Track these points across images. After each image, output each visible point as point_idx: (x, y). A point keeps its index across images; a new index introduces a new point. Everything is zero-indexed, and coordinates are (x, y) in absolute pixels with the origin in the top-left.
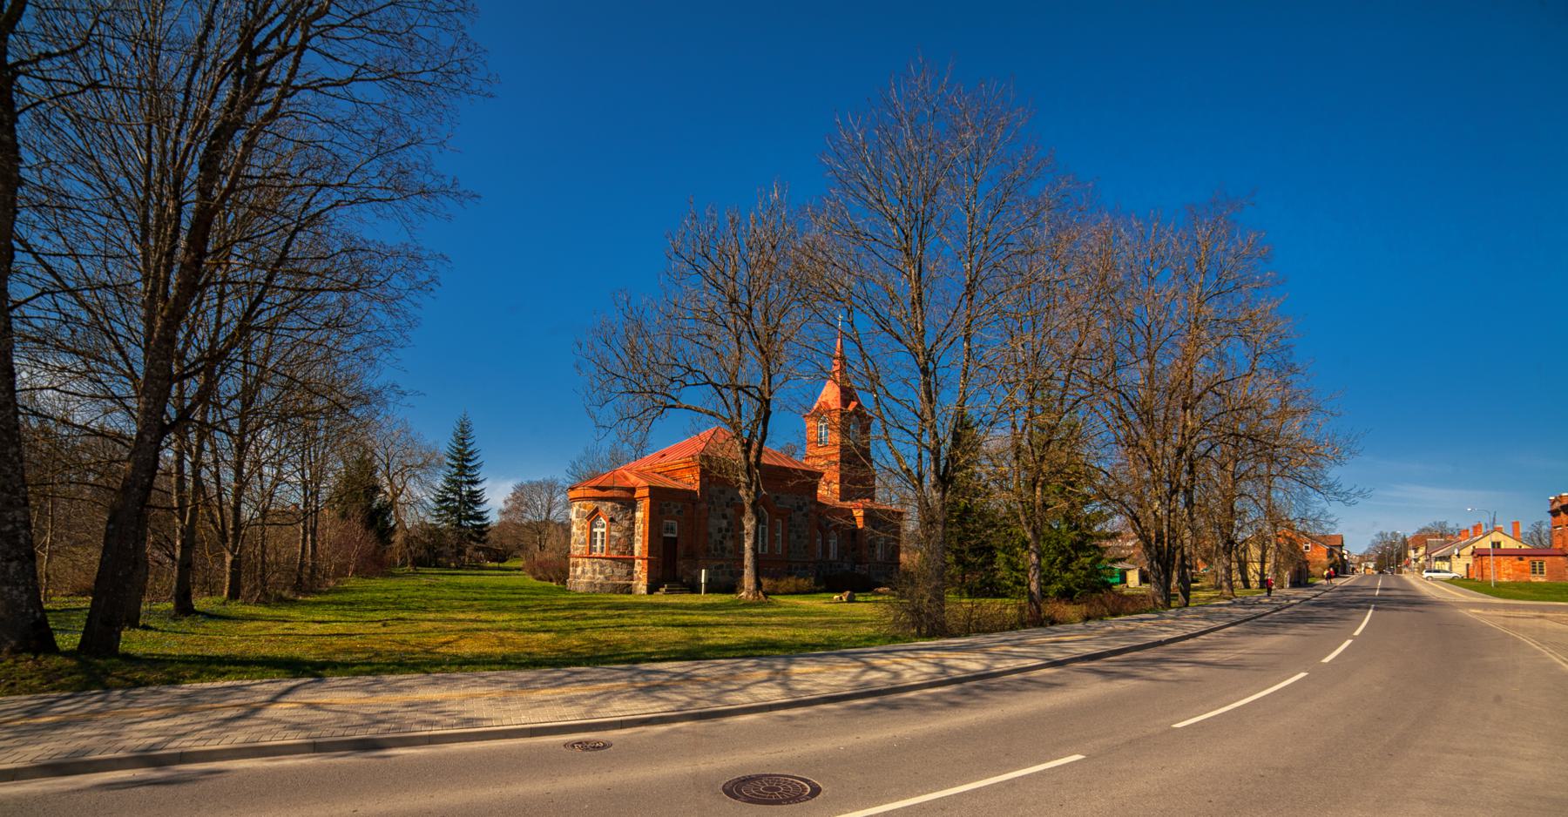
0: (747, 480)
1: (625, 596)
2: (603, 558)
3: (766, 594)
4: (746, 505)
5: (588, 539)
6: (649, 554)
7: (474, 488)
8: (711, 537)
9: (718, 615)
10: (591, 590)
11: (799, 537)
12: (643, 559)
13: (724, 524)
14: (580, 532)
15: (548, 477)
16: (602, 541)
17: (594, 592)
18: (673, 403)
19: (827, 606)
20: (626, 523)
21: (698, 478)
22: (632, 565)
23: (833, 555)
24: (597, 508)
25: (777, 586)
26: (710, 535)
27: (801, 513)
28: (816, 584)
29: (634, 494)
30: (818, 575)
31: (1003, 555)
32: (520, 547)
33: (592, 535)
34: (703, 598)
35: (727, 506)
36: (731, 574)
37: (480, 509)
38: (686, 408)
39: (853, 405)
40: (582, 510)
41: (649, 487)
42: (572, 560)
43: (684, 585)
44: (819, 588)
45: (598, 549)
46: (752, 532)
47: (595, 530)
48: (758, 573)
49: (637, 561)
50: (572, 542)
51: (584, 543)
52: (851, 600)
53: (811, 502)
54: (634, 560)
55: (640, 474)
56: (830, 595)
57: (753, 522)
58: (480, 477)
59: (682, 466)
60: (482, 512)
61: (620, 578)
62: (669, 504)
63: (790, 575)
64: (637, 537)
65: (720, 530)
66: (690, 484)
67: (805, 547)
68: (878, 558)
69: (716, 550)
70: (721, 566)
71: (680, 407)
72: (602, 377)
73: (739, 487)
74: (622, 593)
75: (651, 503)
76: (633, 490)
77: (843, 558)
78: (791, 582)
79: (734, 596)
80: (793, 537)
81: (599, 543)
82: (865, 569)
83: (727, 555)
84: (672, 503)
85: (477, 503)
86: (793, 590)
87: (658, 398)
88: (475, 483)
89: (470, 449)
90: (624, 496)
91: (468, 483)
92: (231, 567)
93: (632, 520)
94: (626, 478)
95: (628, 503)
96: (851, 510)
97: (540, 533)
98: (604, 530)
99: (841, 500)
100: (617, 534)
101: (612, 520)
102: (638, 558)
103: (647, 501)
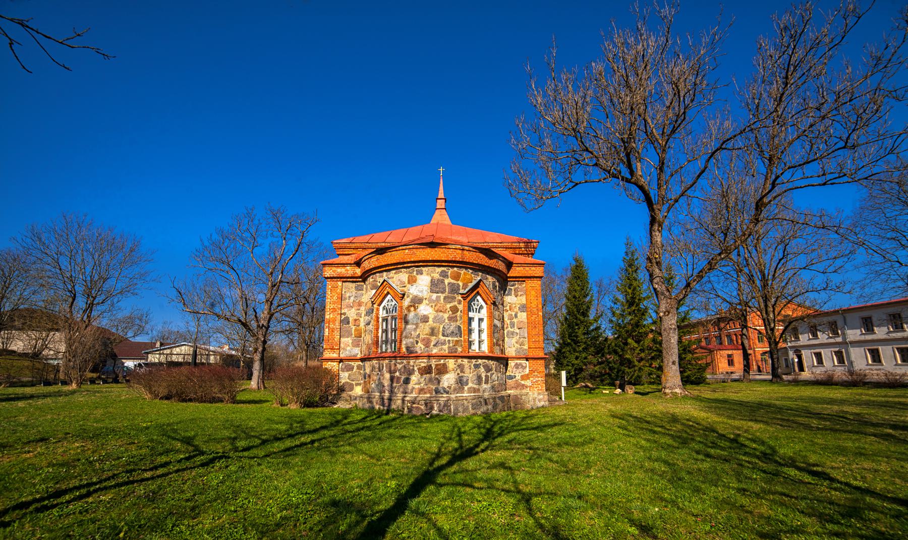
47: (471, 314)
49: (512, 363)
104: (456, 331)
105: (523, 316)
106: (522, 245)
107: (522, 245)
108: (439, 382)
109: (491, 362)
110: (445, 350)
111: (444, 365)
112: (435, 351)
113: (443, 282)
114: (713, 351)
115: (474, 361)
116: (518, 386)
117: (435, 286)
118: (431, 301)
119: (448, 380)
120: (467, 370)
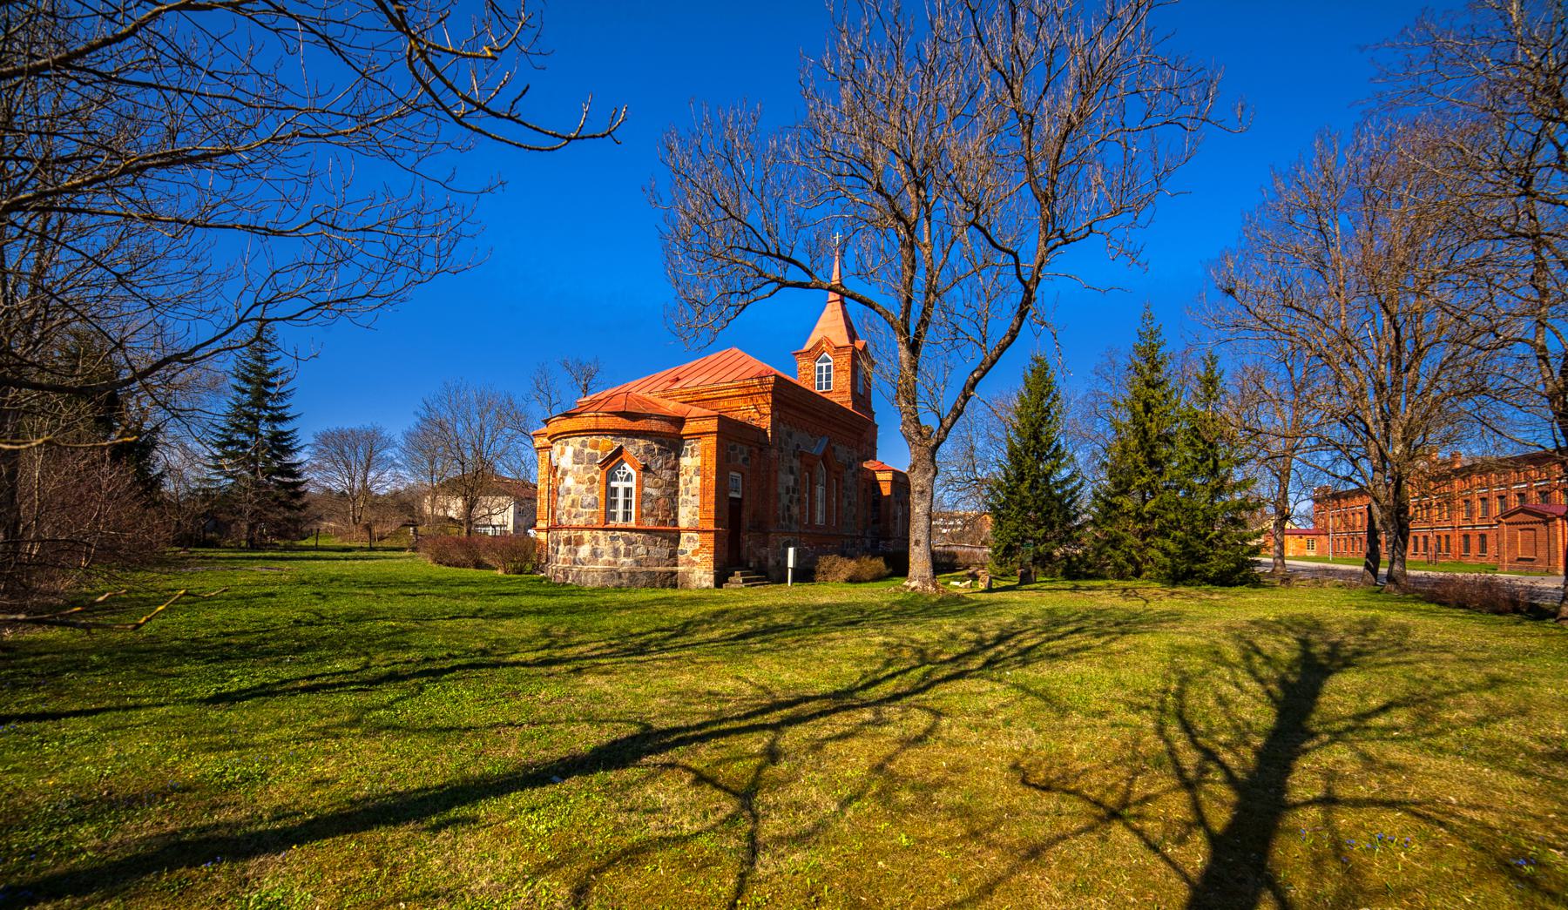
5: (602, 499)
7: (280, 427)
14: (583, 487)
16: (627, 504)
20: (667, 475)
21: (767, 410)
22: (676, 541)
24: (621, 448)
29: (681, 428)
37: (288, 460)
45: (620, 517)
47: (613, 484)
49: (684, 536)
51: (596, 504)
54: (678, 532)
58: (290, 412)
59: (732, 392)
61: (659, 562)
74: (663, 586)
75: (718, 443)
76: (680, 421)
85: (288, 451)
88: (282, 419)
89: (271, 369)
90: (666, 430)
91: (272, 419)
92: (616, 501)
95: (671, 441)
96: (873, 473)
100: (654, 492)
102: (688, 530)
103: (711, 441)
104: (593, 502)
105: (697, 480)
106: (756, 382)
107: (756, 382)
108: (576, 552)
109: (635, 535)
110: (581, 521)
111: (581, 536)
112: (575, 523)
113: (582, 452)
114: (1553, 519)
115: (610, 533)
116: (690, 562)
117: (577, 456)
118: (574, 473)
119: (584, 551)
120: (602, 542)
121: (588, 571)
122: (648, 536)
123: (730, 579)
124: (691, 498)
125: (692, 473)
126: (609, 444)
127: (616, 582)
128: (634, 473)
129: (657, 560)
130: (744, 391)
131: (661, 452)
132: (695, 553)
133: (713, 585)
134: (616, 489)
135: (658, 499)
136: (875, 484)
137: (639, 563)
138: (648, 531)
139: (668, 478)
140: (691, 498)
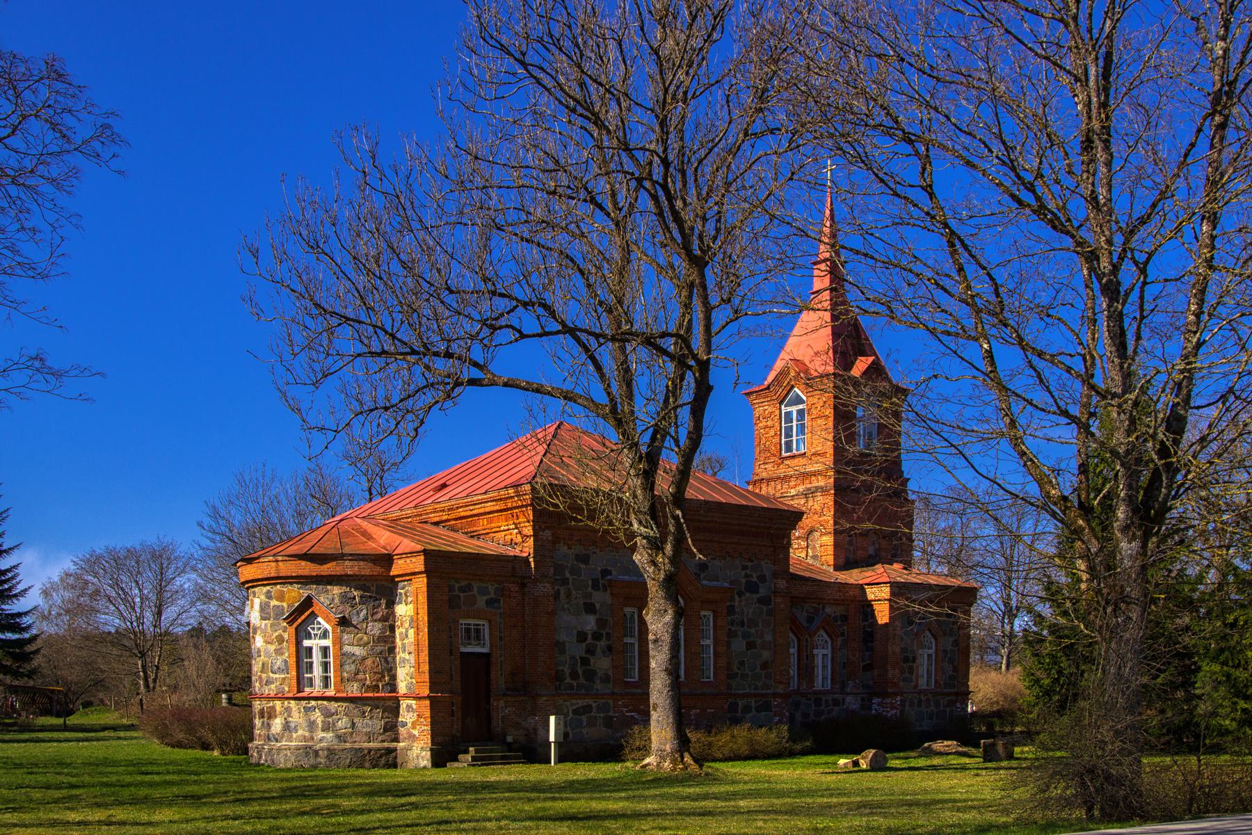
0: (653, 532)
1: (384, 772)
2: (329, 699)
3: (699, 761)
4: (650, 583)
5: (292, 662)
6: (433, 686)
8: (563, 651)
9: (627, 799)
10: (306, 762)
11: (751, 645)
12: (418, 698)
13: (590, 623)
14: (272, 648)
15: (152, 540)
16: (326, 666)
17: (315, 767)
18: (476, 373)
19: (830, 778)
20: (375, 628)
21: (528, 530)
22: (395, 711)
23: (822, 679)
25: (710, 744)
26: (560, 647)
27: (756, 596)
28: (793, 738)
30: (791, 720)
31: (1216, 668)
32: (99, 684)
33: (302, 655)
34: (555, 771)
35: (595, 586)
36: (609, 722)
38: (506, 385)
39: (861, 366)
40: (274, 603)
41: (425, 552)
42: (257, 705)
43: (510, 747)
44: (798, 747)
45: (318, 682)
46: (667, 638)
47: (307, 643)
48: (681, 724)
49: (404, 704)
50: (256, 668)
52: (877, 766)
53: (775, 575)
54: (397, 701)
55: (394, 525)
56: (830, 759)
57: (668, 618)
59: (489, 507)
60: (20, 615)
62: (469, 588)
63: (736, 721)
64: (401, 655)
65: (582, 637)
66: (512, 543)
67: (765, 666)
68: (922, 683)
69: (574, 675)
70: (588, 709)
71: (493, 384)
72: (310, 323)
73: (633, 549)
75: (429, 585)
76: (386, 560)
77: (843, 686)
78: (741, 735)
79: (618, 767)
80: (739, 645)
81: (317, 671)
82: (893, 708)
83: (598, 686)
84: (475, 585)
86: (745, 750)
87: (440, 365)
92: (311, 663)
93: (389, 622)
94: (368, 536)
96: (861, 588)
97: (143, 655)
98: (327, 643)
99: (835, 569)
100: (358, 651)
101: (344, 622)
102: (406, 696)
103: (421, 583)
108: (269, 726)
111: (273, 708)
115: (304, 703)
117: (265, 607)
120: (295, 714)
121: (279, 749)
122: (352, 706)
123: (461, 756)
124: (407, 657)
125: (407, 625)
126: (295, 594)
127: (312, 761)
128: (329, 628)
129: (368, 734)
130: (501, 506)
131: (364, 600)
132: (414, 725)
133: (429, 765)
134: (310, 649)
135: (364, 659)
136: (867, 608)
137: (341, 738)
138: (351, 700)
139: (377, 632)
140: (407, 657)
